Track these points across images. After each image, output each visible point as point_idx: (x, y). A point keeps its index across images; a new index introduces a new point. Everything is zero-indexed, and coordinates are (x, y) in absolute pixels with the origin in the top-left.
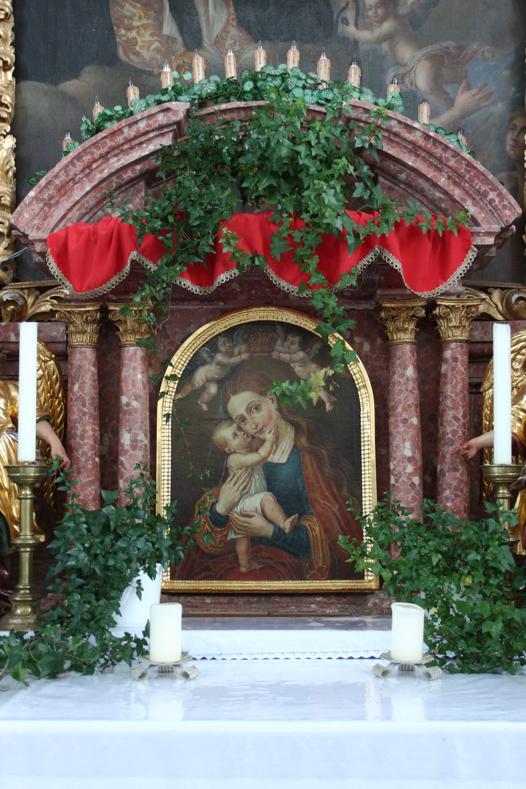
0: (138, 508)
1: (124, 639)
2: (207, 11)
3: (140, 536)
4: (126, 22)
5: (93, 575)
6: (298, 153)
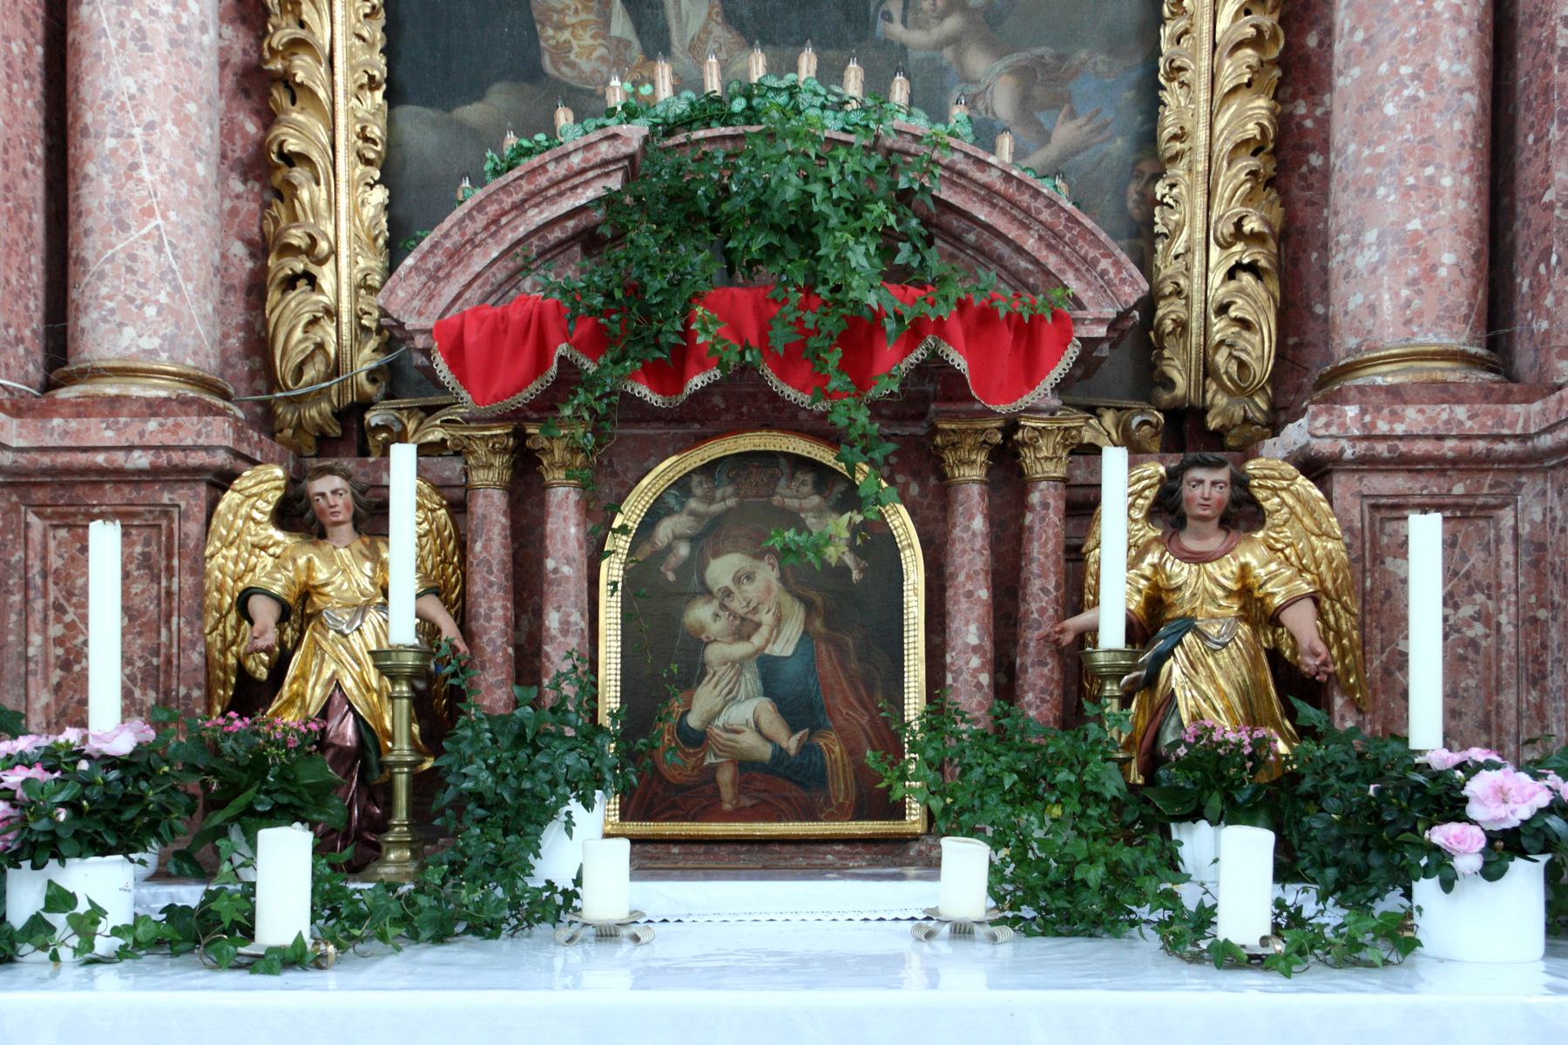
0: (567, 711)
1: (545, 889)
3: (571, 750)
4: (555, 17)
5: (500, 804)
6: (813, 195)
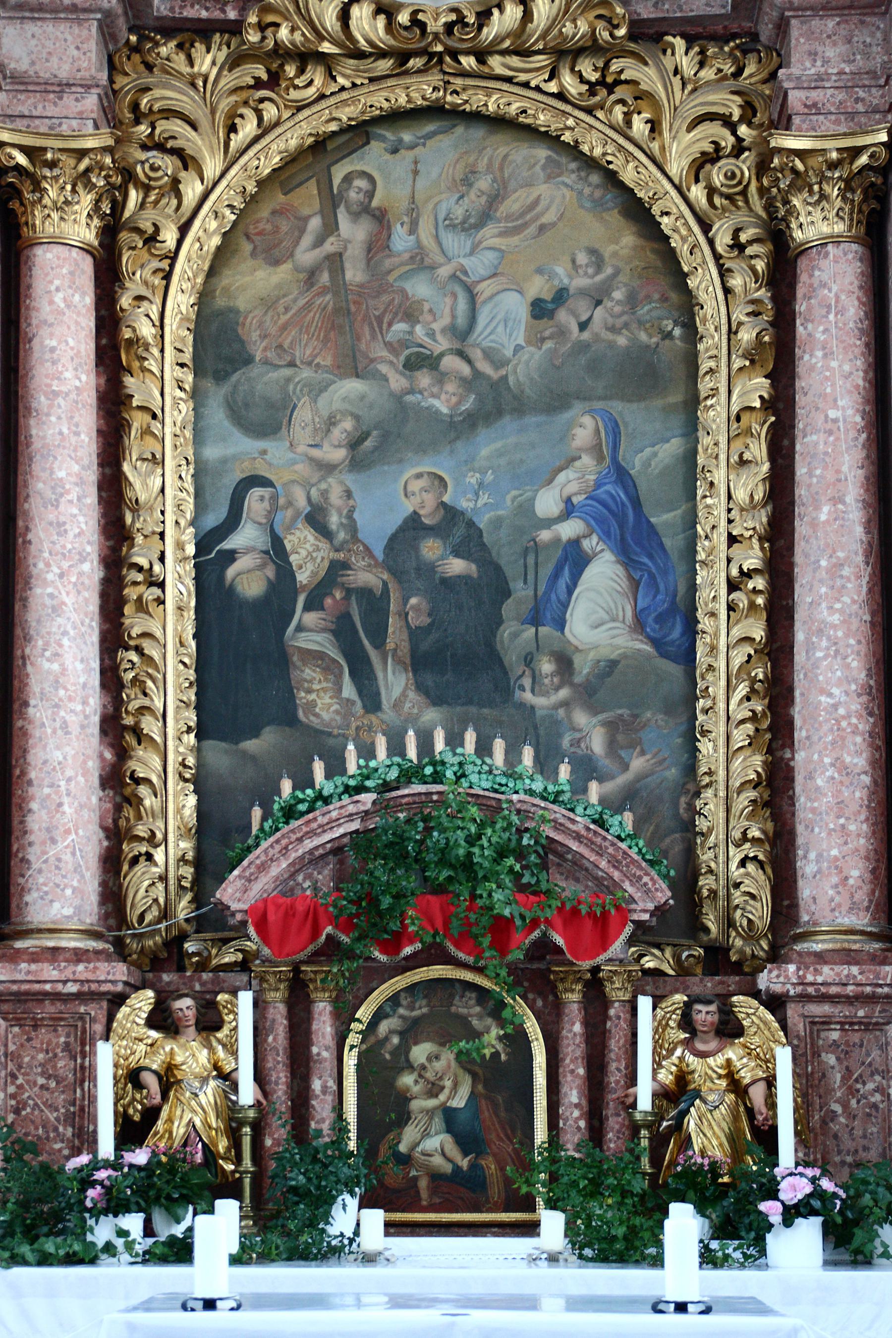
2: (386, 677)
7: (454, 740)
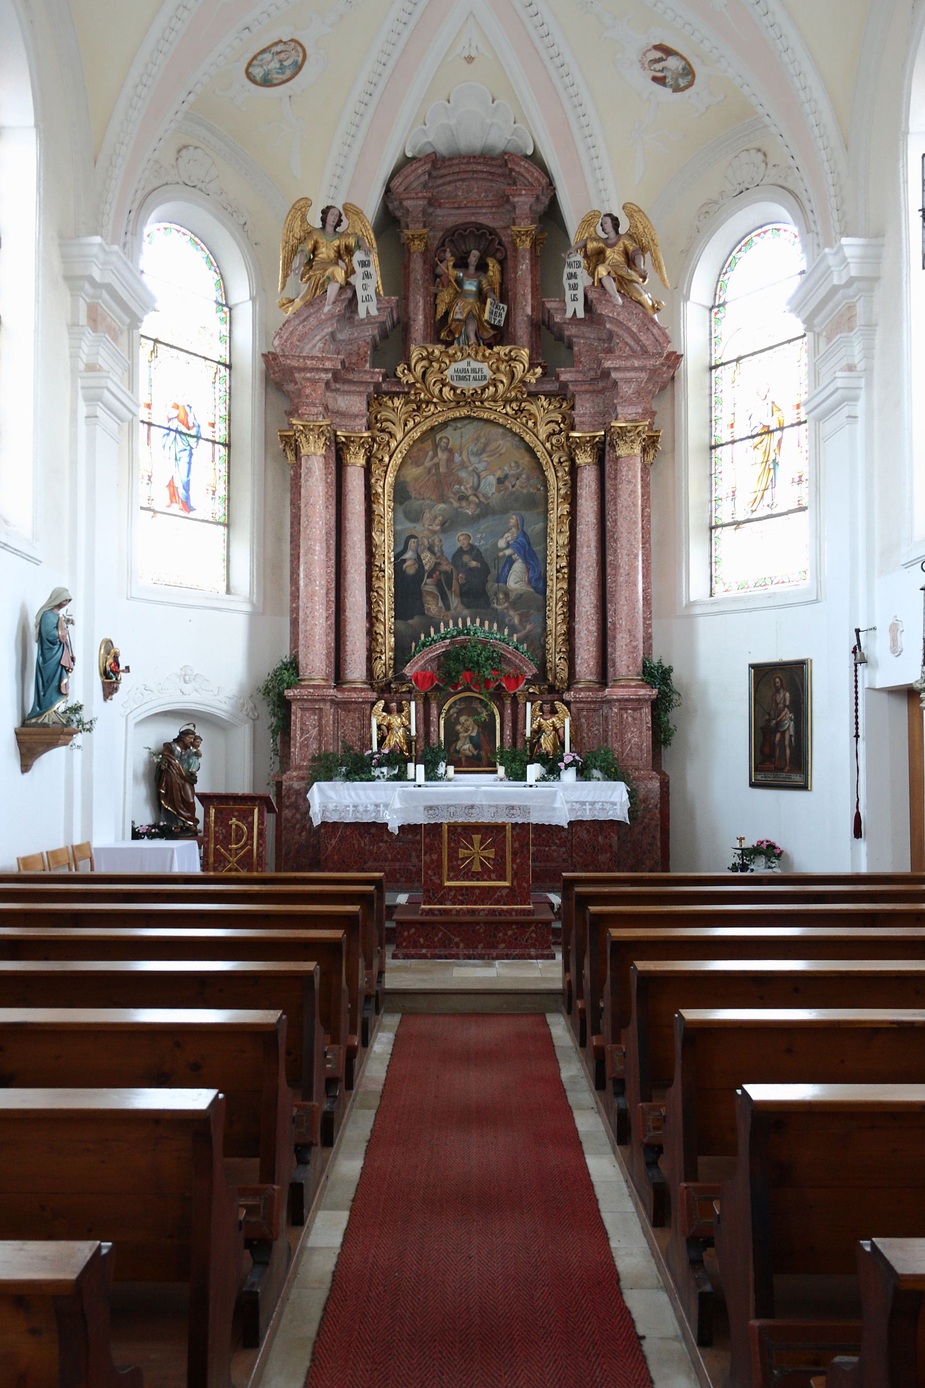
7: (473, 622)
